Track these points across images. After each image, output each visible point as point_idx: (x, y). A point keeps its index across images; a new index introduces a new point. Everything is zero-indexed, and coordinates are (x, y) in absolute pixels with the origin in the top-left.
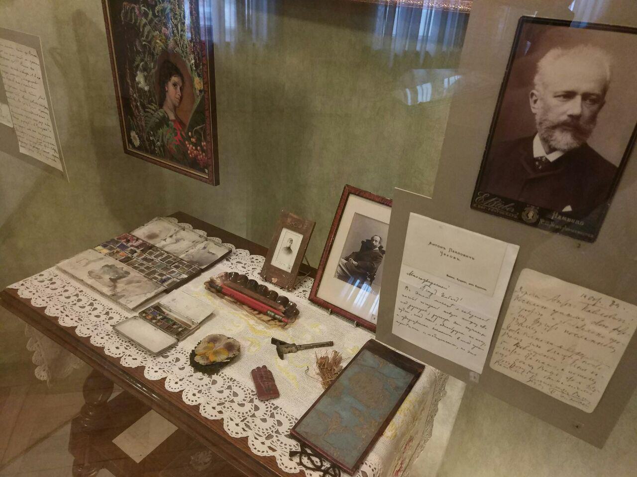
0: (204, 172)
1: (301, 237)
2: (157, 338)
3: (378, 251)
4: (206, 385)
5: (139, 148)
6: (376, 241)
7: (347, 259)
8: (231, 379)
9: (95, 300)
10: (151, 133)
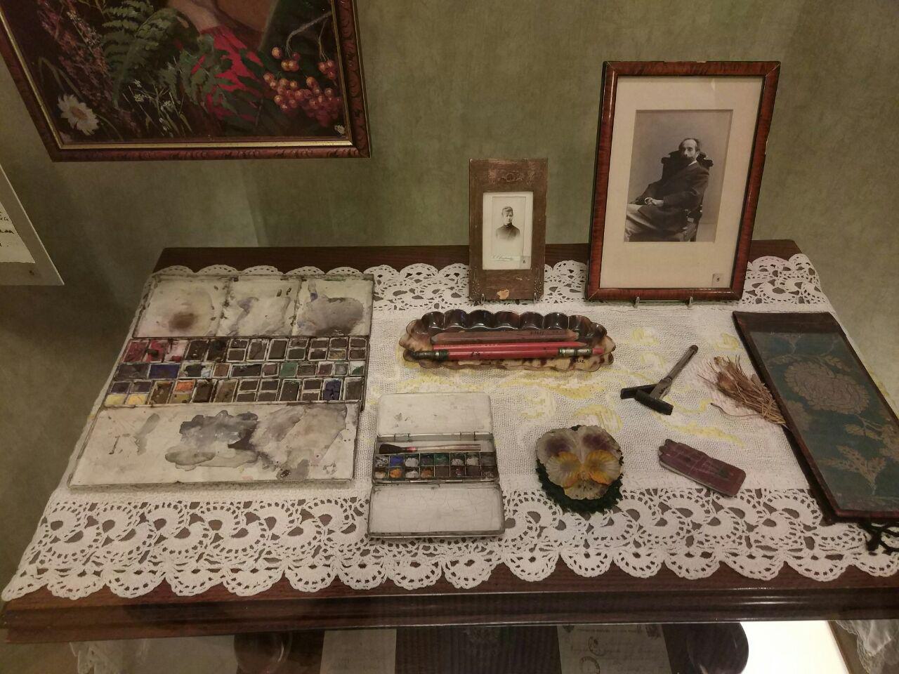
0: (338, 136)
1: (528, 197)
2: (456, 504)
3: (698, 166)
4: (96, 541)
5: (99, 135)
6: (690, 149)
7: (640, 201)
8: (648, 491)
9: (93, 507)
10: (134, 86)
